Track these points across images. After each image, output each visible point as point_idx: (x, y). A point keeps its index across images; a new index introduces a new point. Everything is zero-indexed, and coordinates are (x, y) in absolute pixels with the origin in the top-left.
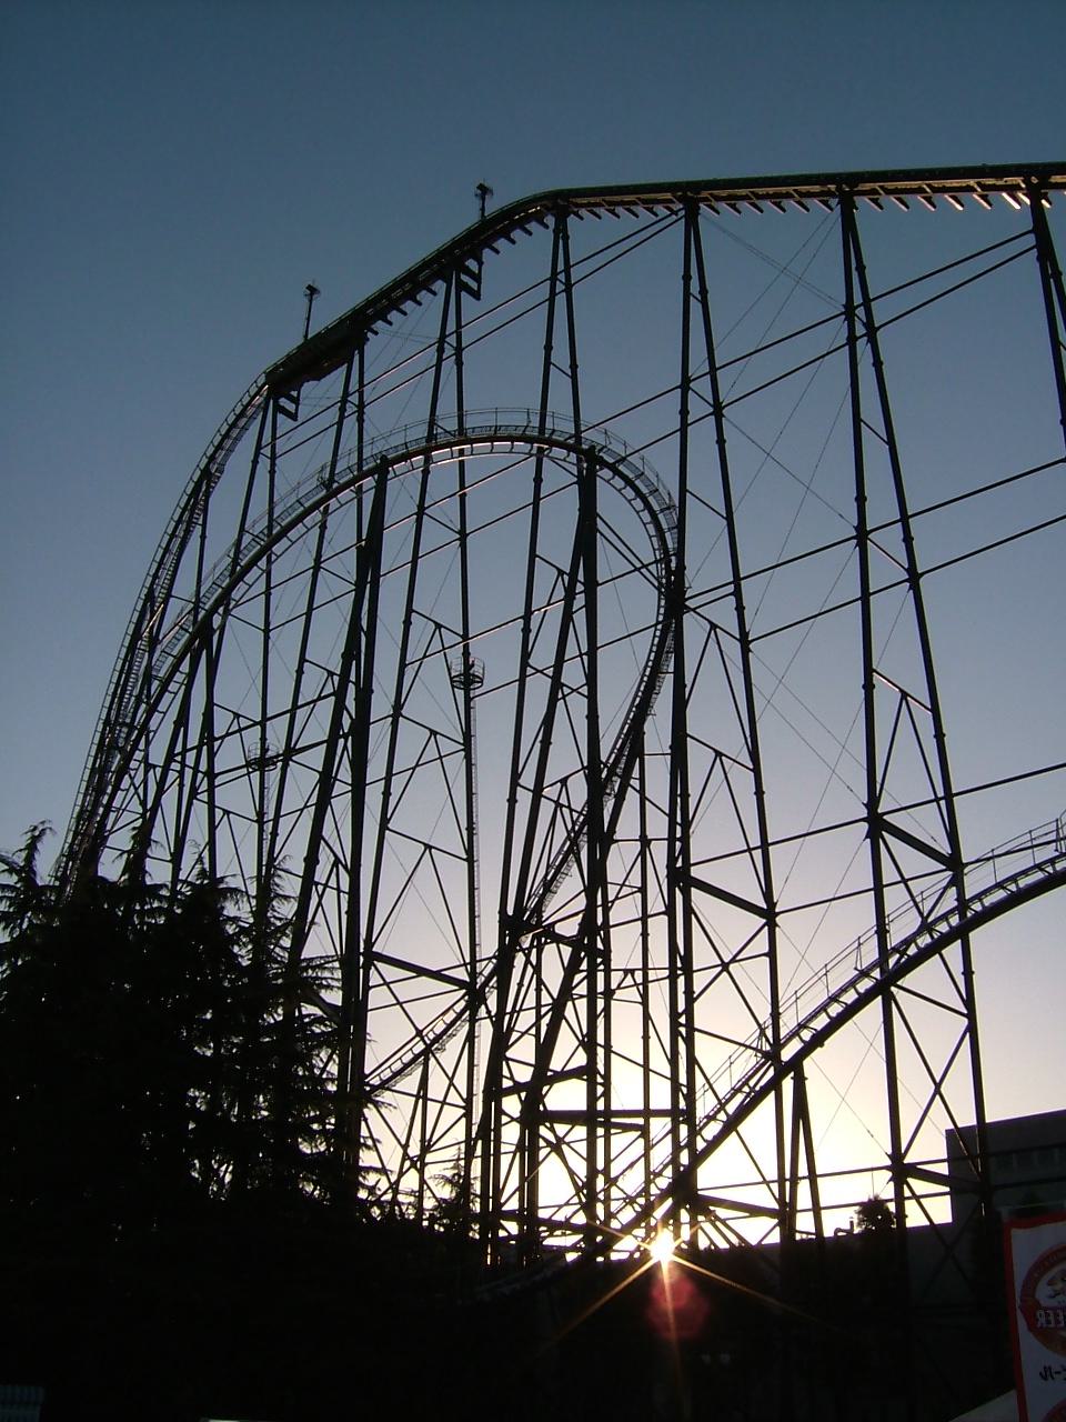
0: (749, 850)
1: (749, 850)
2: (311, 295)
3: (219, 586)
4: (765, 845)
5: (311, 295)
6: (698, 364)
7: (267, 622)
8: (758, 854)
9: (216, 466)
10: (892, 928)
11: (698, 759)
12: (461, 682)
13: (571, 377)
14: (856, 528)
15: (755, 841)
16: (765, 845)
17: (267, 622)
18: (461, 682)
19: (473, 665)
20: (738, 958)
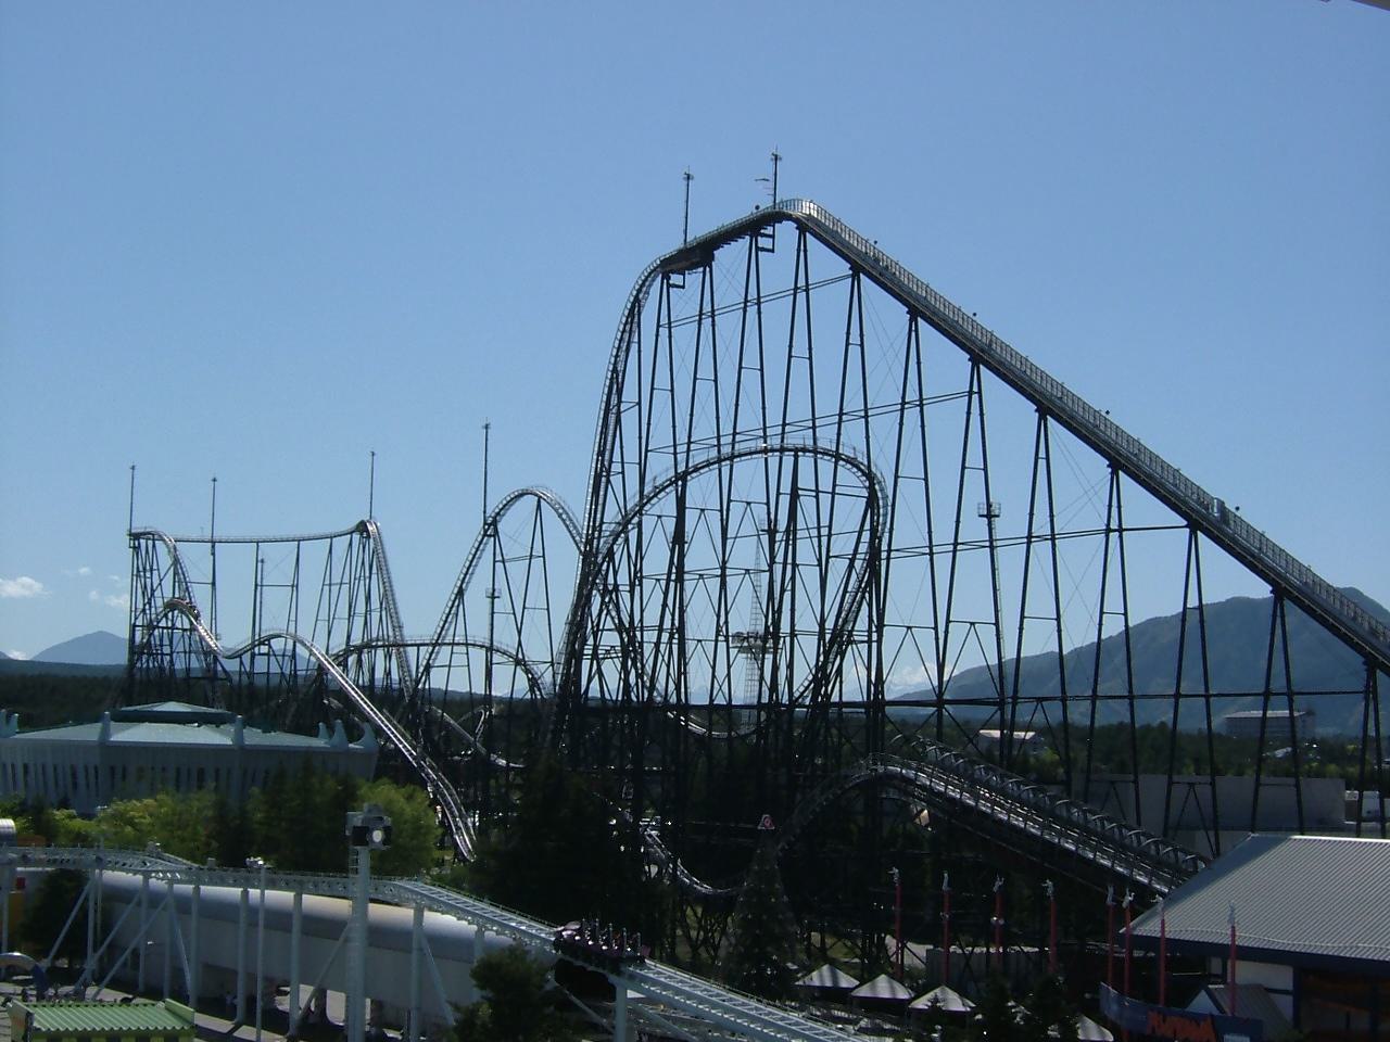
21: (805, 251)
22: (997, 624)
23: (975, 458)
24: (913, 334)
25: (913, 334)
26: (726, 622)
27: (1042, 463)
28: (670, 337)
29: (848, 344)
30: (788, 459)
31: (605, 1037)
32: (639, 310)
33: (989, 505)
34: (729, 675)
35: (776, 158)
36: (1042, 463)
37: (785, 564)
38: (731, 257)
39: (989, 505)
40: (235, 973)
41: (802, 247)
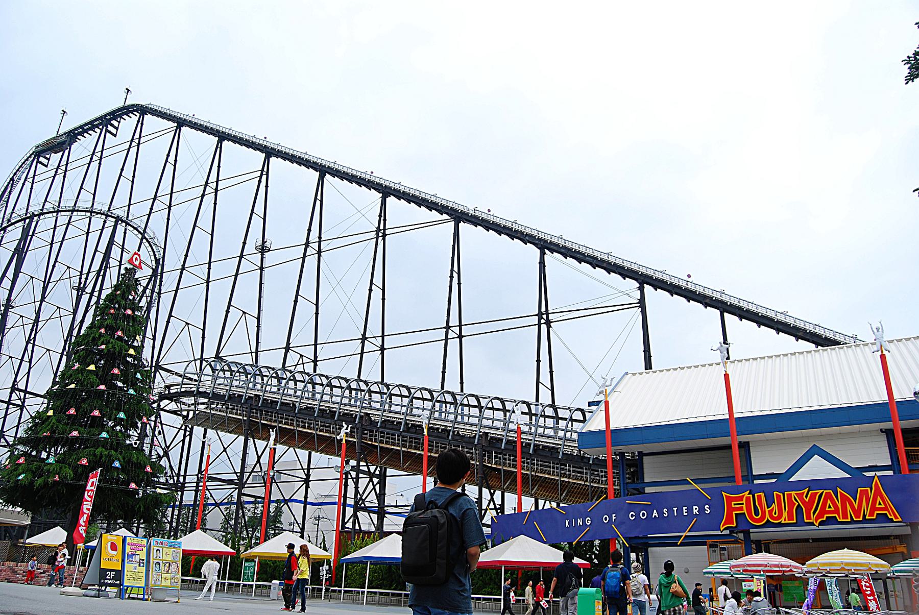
0: (251, 353)
1: (251, 353)
2: (128, 92)
3: (4, 201)
4: (257, 352)
5: (128, 92)
6: (314, 237)
7: (316, 357)
8: (254, 355)
9: (17, 177)
10: (30, 208)
11: (234, 314)
12: (260, 249)
13: (320, 201)
14: (551, 327)
15: (254, 350)
16: (257, 352)
17: (316, 357)
18: (260, 249)
19: (266, 242)
20: (275, 461)
21: (142, 124)
22: (258, 319)
23: (259, 209)
24: (219, 149)
25: (219, 149)
26: (35, 338)
27: (318, 203)
28: (31, 189)
29: (167, 161)
30: (111, 222)
31: (3, 537)
32: (11, 189)
33: (264, 242)
34: (29, 373)
35: (128, 90)
36: (318, 203)
37: (92, 294)
38: (83, 147)
39: (264, 242)
40: (421, 426)
41: (141, 121)
